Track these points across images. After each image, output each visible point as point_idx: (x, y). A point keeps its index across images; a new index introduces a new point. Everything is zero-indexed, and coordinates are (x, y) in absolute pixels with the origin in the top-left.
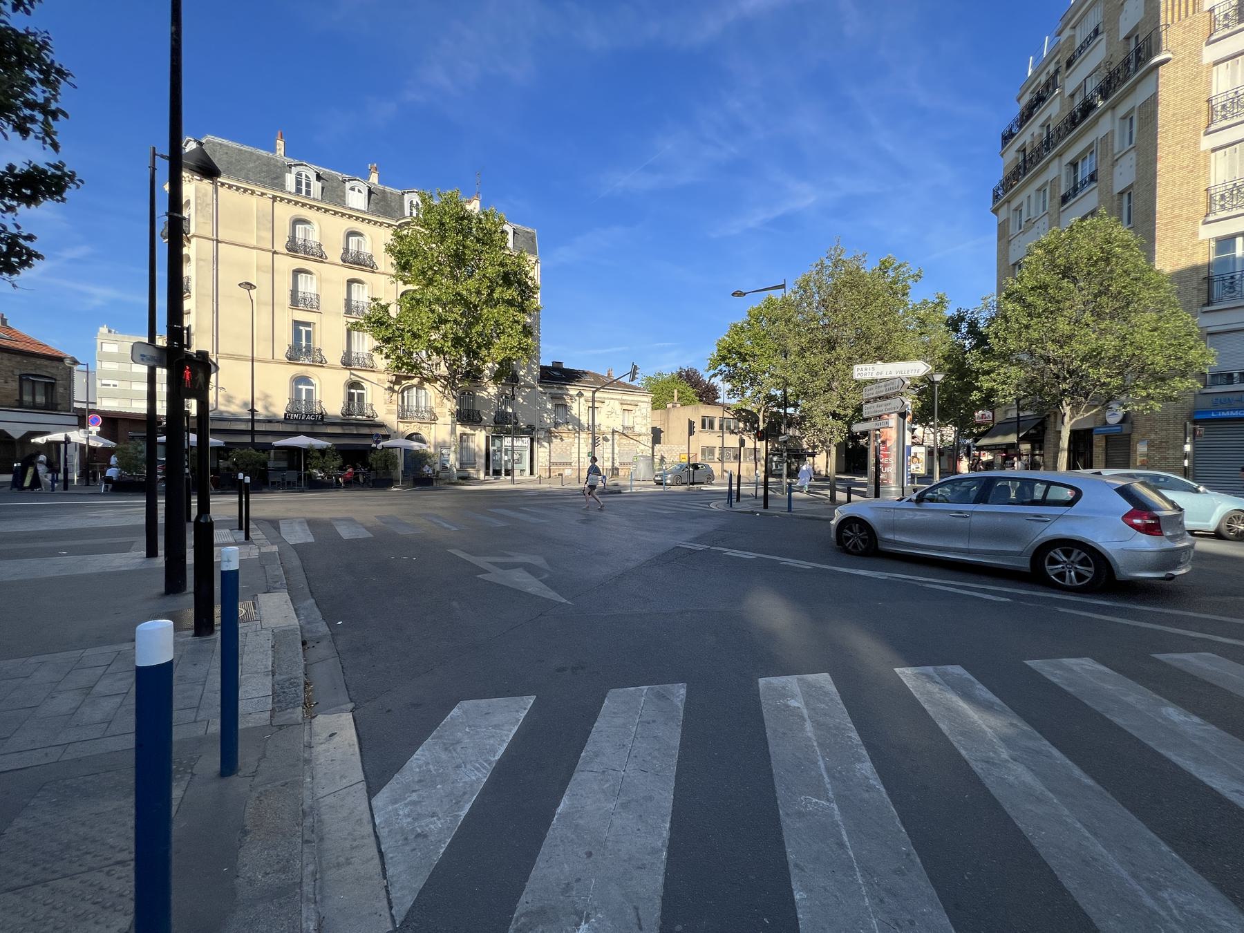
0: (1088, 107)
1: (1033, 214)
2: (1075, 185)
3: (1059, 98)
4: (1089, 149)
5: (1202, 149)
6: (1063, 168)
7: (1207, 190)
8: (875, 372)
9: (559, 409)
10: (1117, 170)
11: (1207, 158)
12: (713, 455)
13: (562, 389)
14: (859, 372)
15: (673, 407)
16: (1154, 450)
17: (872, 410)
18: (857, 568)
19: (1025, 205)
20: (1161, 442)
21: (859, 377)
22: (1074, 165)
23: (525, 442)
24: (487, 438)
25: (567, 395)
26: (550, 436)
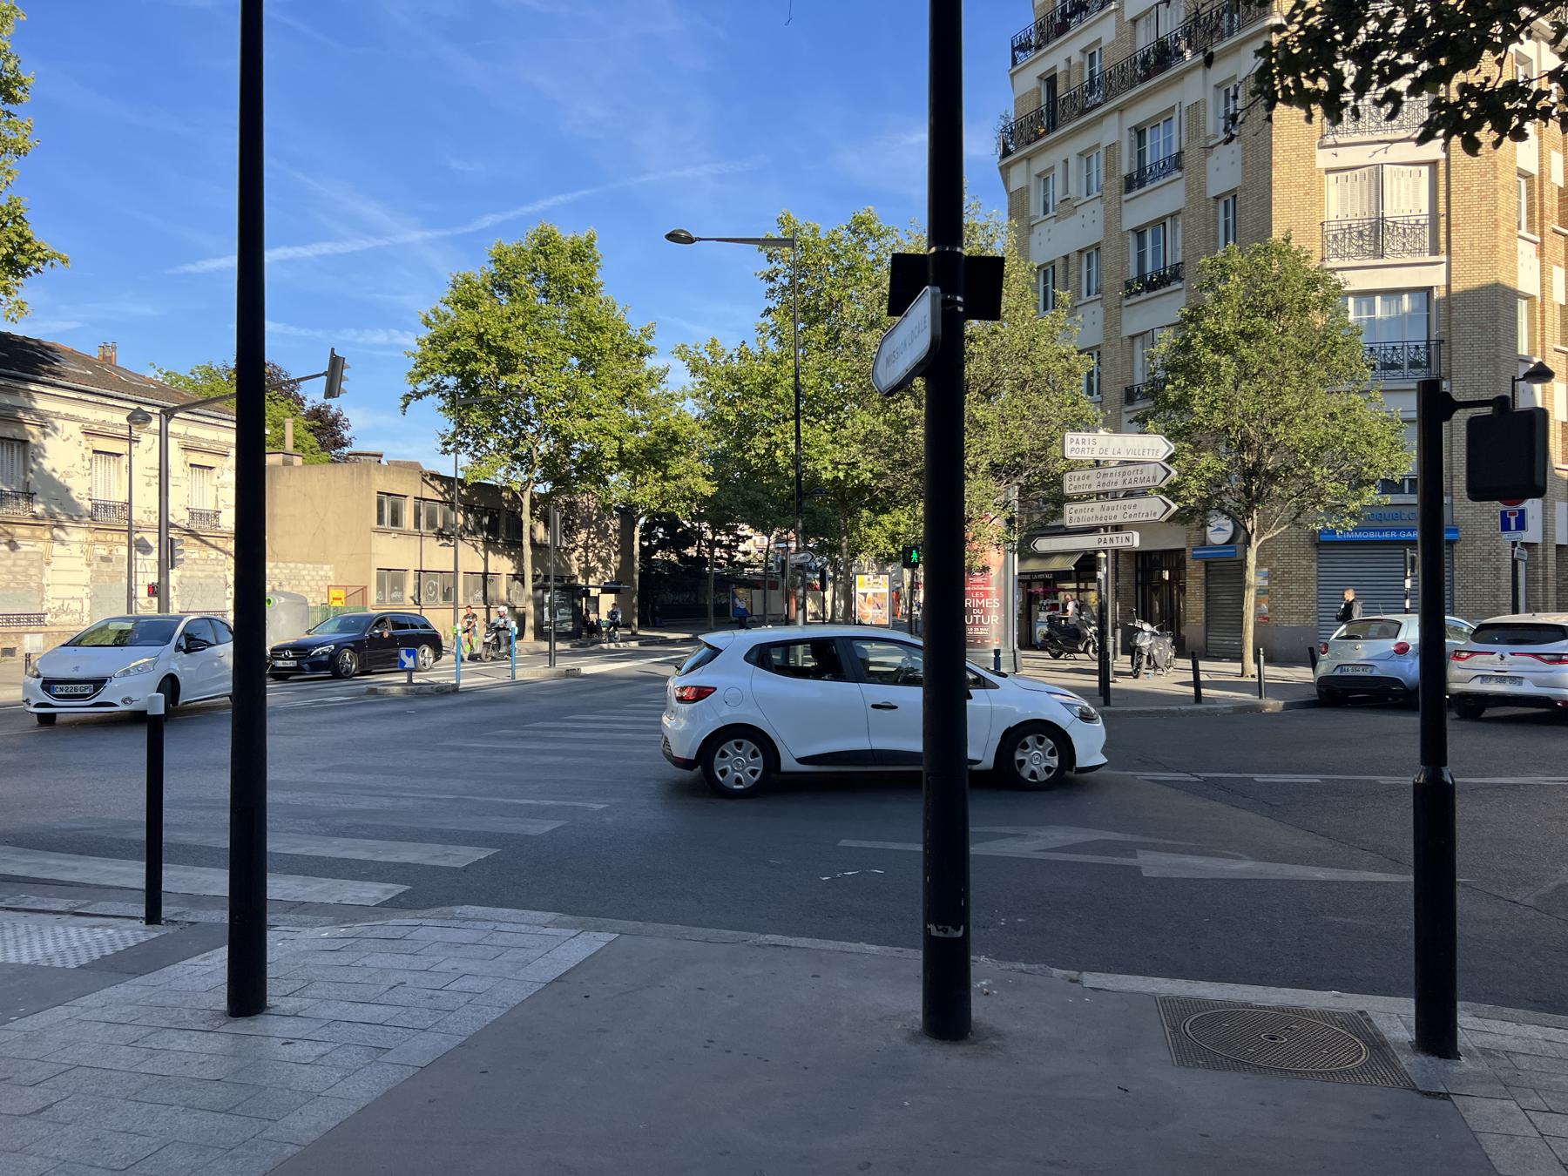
1: (1073, 193)
3: (1113, 17)
4: (1166, 116)
5: (1318, 166)
6: (1126, 133)
7: (1322, 224)
8: (1097, 448)
10: (1212, 161)
11: (1321, 181)
12: (401, 589)
14: (1074, 445)
15: (285, 463)
16: (1275, 584)
17: (1090, 514)
19: (1059, 172)
20: (1284, 572)
21: (1074, 454)
22: (1139, 132)
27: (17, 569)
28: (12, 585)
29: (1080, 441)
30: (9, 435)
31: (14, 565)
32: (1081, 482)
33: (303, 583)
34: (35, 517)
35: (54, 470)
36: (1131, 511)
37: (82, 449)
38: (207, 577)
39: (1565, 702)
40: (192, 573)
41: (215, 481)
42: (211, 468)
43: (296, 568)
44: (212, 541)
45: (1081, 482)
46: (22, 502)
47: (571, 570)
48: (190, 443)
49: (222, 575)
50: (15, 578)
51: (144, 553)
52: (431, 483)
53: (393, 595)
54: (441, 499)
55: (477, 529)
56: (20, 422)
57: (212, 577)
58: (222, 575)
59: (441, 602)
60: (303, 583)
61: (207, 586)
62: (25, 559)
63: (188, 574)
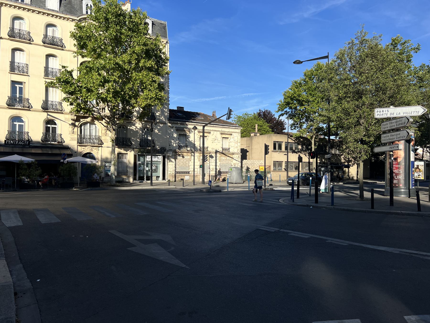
12: (281, 166)
15: (255, 135)
17: (388, 138)
27: (184, 162)
28: (183, 165)
29: (381, 112)
30: (182, 133)
31: (183, 161)
32: (386, 126)
33: (255, 165)
34: (188, 151)
35: (192, 141)
36: (398, 136)
37: (198, 136)
38: (226, 163)
39: (1, 190)
40: (223, 163)
41: (229, 141)
42: (228, 138)
43: (253, 161)
44: (228, 155)
45: (386, 126)
46: (186, 148)
47: (341, 161)
48: (222, 132)
49: (230, 163)
50: (183, 164)
51: (211, 158)
52: (291, 138)
53: (279, 168)
54: (294, 142)
55: (307, 150)
56: (185, 131)
57: (228, 163)
58: (230, 163)
59: (294, 170)
60: (255, 165)
61: (227, 165)
62: (186, 160)
63: (222, 163)
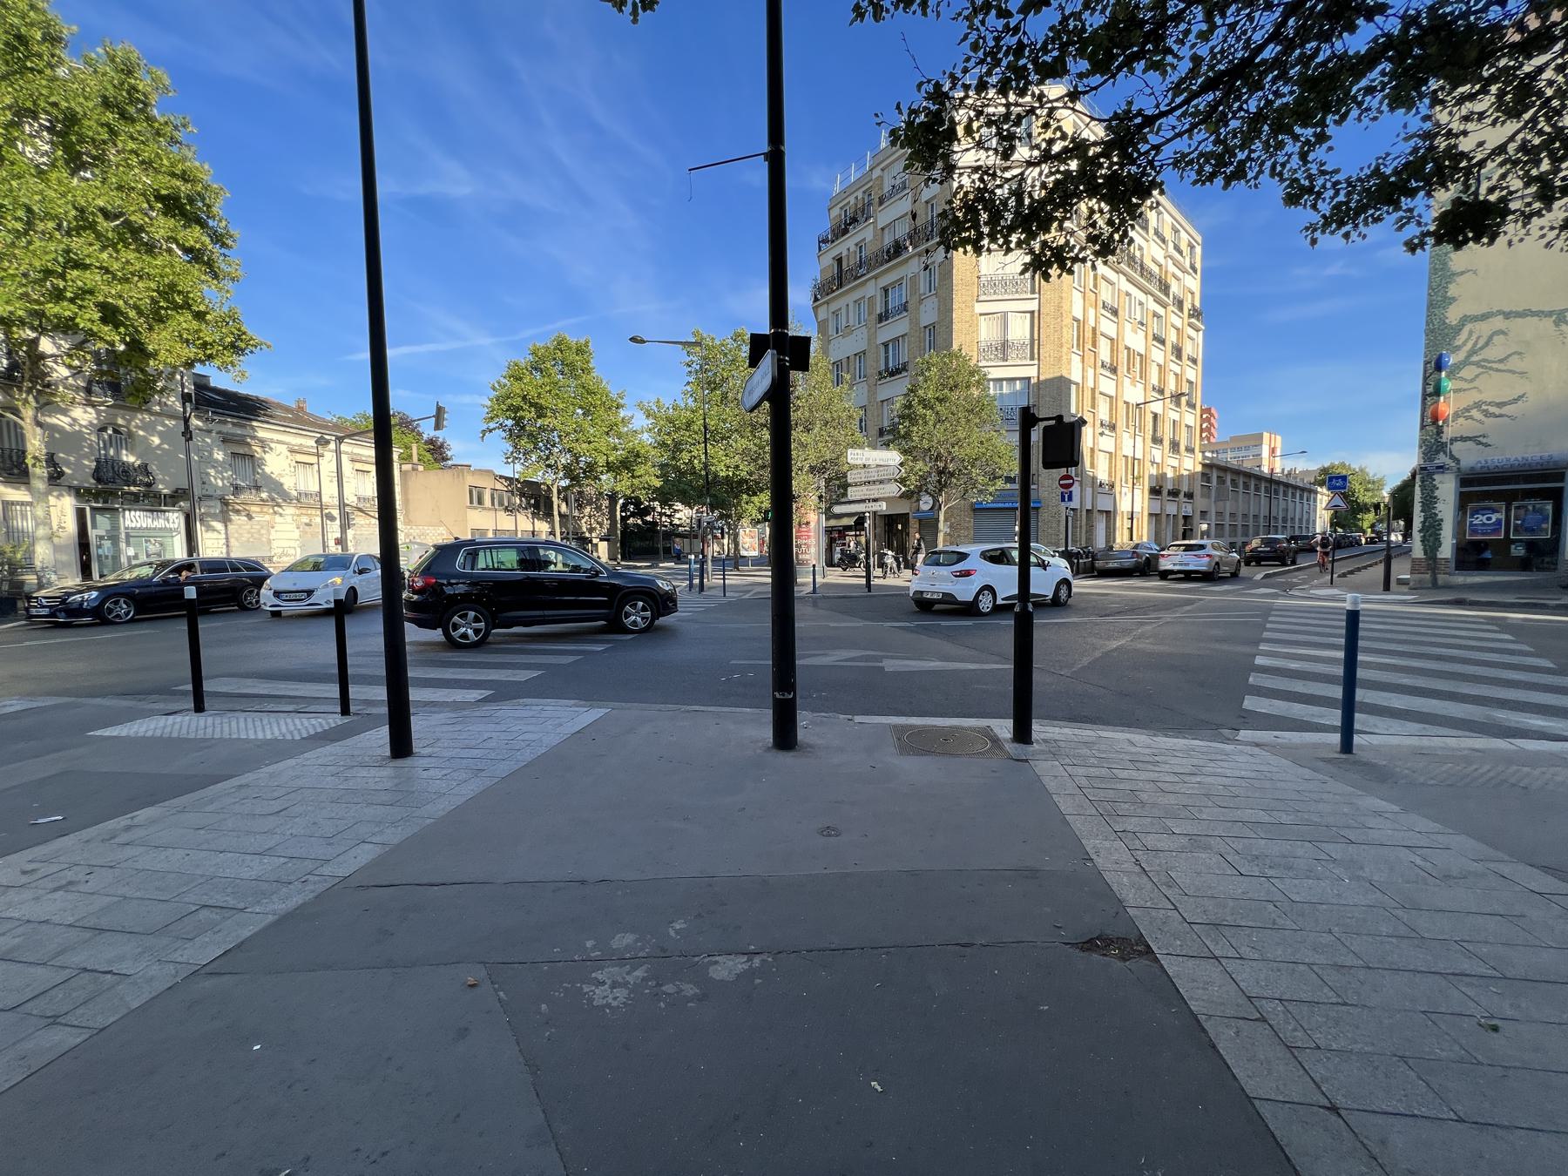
0: (897, 249)
1: (851, 323)
2: (887, 311)
4: (899, 282)
9: (239, 462)
10: (922, 307)
13: (244, 426)
15: (413, 469)
18: (1144, 597)
23: (175, 519)
24: (81, 514)
25: (254, 438)
26: (226, 511)
